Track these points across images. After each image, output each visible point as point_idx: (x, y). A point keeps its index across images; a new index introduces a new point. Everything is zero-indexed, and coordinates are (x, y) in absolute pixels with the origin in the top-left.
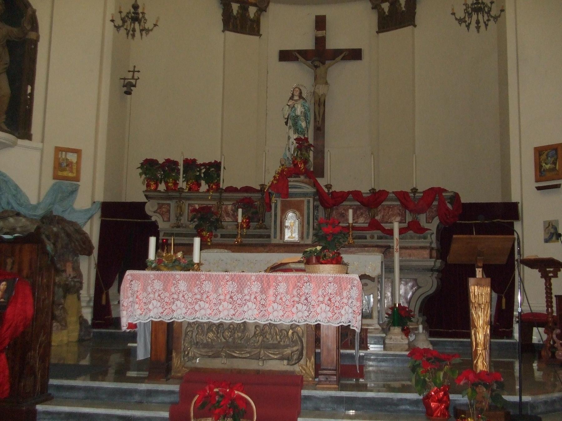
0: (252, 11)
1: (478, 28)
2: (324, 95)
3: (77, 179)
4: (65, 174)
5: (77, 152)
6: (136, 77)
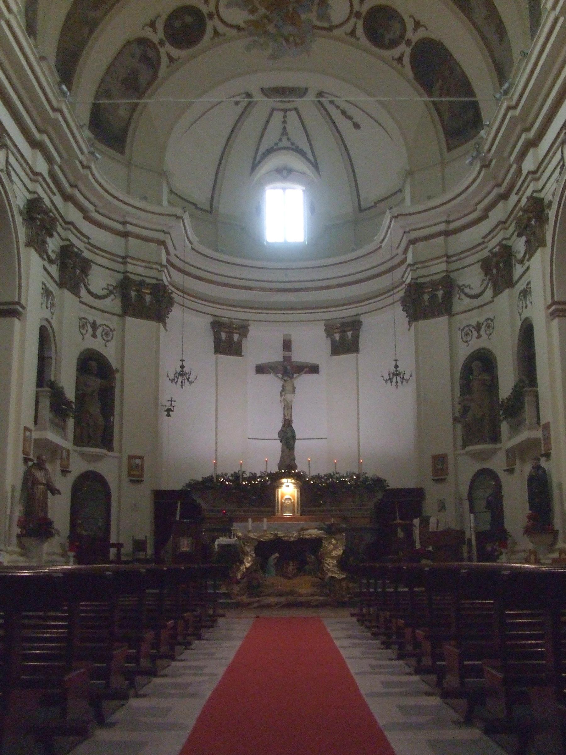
0: (236, 337)
1: (397, 386)
2: (291, 401)
3: (142, 476)
4: (134, 473)
5: (141, 458)
6: (173, 405)
